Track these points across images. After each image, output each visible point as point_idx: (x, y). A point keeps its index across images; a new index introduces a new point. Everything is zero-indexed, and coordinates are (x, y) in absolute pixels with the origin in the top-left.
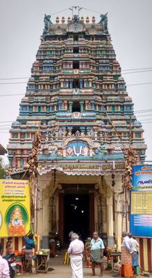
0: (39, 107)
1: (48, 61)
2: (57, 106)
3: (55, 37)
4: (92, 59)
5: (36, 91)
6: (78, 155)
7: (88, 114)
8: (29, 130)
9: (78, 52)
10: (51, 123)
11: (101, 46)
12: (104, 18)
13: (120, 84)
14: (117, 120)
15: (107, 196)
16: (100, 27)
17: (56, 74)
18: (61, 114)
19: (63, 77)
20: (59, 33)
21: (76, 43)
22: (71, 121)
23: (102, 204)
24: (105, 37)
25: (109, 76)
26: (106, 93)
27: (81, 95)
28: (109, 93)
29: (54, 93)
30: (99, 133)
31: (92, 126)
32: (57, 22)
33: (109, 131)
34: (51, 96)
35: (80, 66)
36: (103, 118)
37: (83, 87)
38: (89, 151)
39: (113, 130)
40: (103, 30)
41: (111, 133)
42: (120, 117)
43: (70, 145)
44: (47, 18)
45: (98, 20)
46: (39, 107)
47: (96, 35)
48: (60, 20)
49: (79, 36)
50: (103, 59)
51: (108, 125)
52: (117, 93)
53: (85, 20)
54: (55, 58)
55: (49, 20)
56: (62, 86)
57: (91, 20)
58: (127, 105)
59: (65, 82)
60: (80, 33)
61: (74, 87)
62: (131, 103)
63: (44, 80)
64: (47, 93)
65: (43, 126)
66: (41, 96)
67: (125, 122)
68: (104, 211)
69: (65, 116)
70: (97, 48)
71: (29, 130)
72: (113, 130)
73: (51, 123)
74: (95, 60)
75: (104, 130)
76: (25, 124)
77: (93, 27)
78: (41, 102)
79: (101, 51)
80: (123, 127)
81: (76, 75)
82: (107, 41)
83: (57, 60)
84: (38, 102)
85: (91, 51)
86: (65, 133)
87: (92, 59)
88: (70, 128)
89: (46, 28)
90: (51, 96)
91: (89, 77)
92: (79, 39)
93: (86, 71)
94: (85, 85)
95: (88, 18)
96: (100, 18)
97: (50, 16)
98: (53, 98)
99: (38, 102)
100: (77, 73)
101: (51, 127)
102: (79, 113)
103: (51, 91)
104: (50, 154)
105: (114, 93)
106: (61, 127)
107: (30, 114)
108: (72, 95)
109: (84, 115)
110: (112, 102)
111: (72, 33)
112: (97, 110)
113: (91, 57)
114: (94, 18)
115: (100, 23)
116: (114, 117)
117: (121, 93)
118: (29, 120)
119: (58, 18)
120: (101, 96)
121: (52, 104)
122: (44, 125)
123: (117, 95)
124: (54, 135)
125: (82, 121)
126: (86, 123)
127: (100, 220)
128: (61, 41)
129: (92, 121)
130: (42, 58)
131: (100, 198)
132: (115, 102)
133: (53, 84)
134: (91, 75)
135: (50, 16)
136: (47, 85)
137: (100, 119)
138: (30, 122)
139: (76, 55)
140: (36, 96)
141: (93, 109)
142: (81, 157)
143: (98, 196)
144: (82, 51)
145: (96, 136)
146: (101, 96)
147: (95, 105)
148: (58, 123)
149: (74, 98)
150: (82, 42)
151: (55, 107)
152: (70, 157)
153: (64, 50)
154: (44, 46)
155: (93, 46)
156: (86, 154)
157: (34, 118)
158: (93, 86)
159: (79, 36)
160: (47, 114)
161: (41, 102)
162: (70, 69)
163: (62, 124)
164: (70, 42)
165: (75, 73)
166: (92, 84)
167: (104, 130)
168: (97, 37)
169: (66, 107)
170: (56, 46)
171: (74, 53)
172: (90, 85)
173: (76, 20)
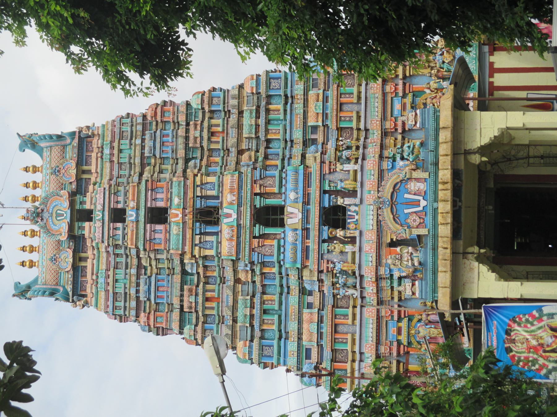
0: (265, 312)
1: (143, 288)
2: (263, 264)
3: (77, 270)
4: (141, 175)
5: (222, 320)
6: (423, 203)
7: (290, 185)
10: (310, 279)
11: (107, 151)
12: (30, 143)
13: (210, 103)
14: (305, 113)
15: (509, 144)
16: (56, 151)
17: (178, 269)
18: (289, 254)
19: (187, 248)
20: (67, 257)
21: (97, 215)
22: (306, 230)
23: (521, 154)
24: (83, 140)
25: (187, 131)
26: (232, 141)
27: (239, 205)
28: (233, 133)
29: (229, 274)
30: (338, 159)
31: (322, 177)
32: (32, 264)
34: (237, 281)
36: (297, 150)
37: (217, 198)
39: (332, 124)
40: (64, 147)
41: (340, 130)
42: (299, 107)
44: (23, 292)
45: (32, 158)
46: (265, 312)
49: (78, 207)
50: (143, 148)
51: (319, 137)
52: (235, 111)
53: (30, 192)
54: (134, 271)
60: (72, 204)
61: (216, 222)
62: (263, 79)
63: (192, 299)
64: (227, 293)
65: (317, 303)
66: (234, 308)
67: (312, 93)
68: (541, 151)
69: (295, 245)
70: (112, 162)
71: (326, 342)
72: (332, 124)
73: (310, 279)
75: (331, 146)
76: (308, 351)
77: (56, 172)
78: (252, 307)
79: (120, 151)
80: (326, 99)
82: (93, 135)
83: (139, 266)
86: (338, 247)
87: (141, 175)
89: (52, 294)
90: (237, 281)
91: (190, 182)
92: (87, 206)
93: (175, 190)
96: (29, 152)
98: (242, 276)
100: (179, 213)
101: (320, 281)
102: (289, 209)
103: (223, 280)
105: (233, 119)
107: (283, 336)
108: (239, 226)
109: (292, 196)
110: (257, 126)
112: (279, 163)
113: (136, 178)
114: (26, 169)
117: (233, 102)
118: (300, 339)
119: (23, 264)
120: (240, 152)
121: (257, 279)
122: (315, 299)
123: (241, 113)
125: (306, 202)
128: (89, 253)
129: (307, 177)
130: (133, 304)
131: (510, 160)
133: (197, 276)
136: (205, 291)
137: (303, 156)
138: (304, 337)
139: (131, 215)
140: (235, 321)
141: (277, 173)
145: (347, 167)
146: (240, 152)
147: (265, 168)
148: (312, 263)
149: (247, 220)
151: (266, 270)
153: (116, 246)
154: (102, 301)
155: (107, 171)
156: (421, 186)
157: (293, 326)
158: (214, 174)
159: (78, 207)
160: (284, 290)
161: (252, 307)
163: (313, 255)
164: (92, 230)
165: (133, 218)
166: (208, 175)
167: (331, 146)
168: (82, 160)
169: (268, 242)
170: (103, 267)
173: (36, 215)
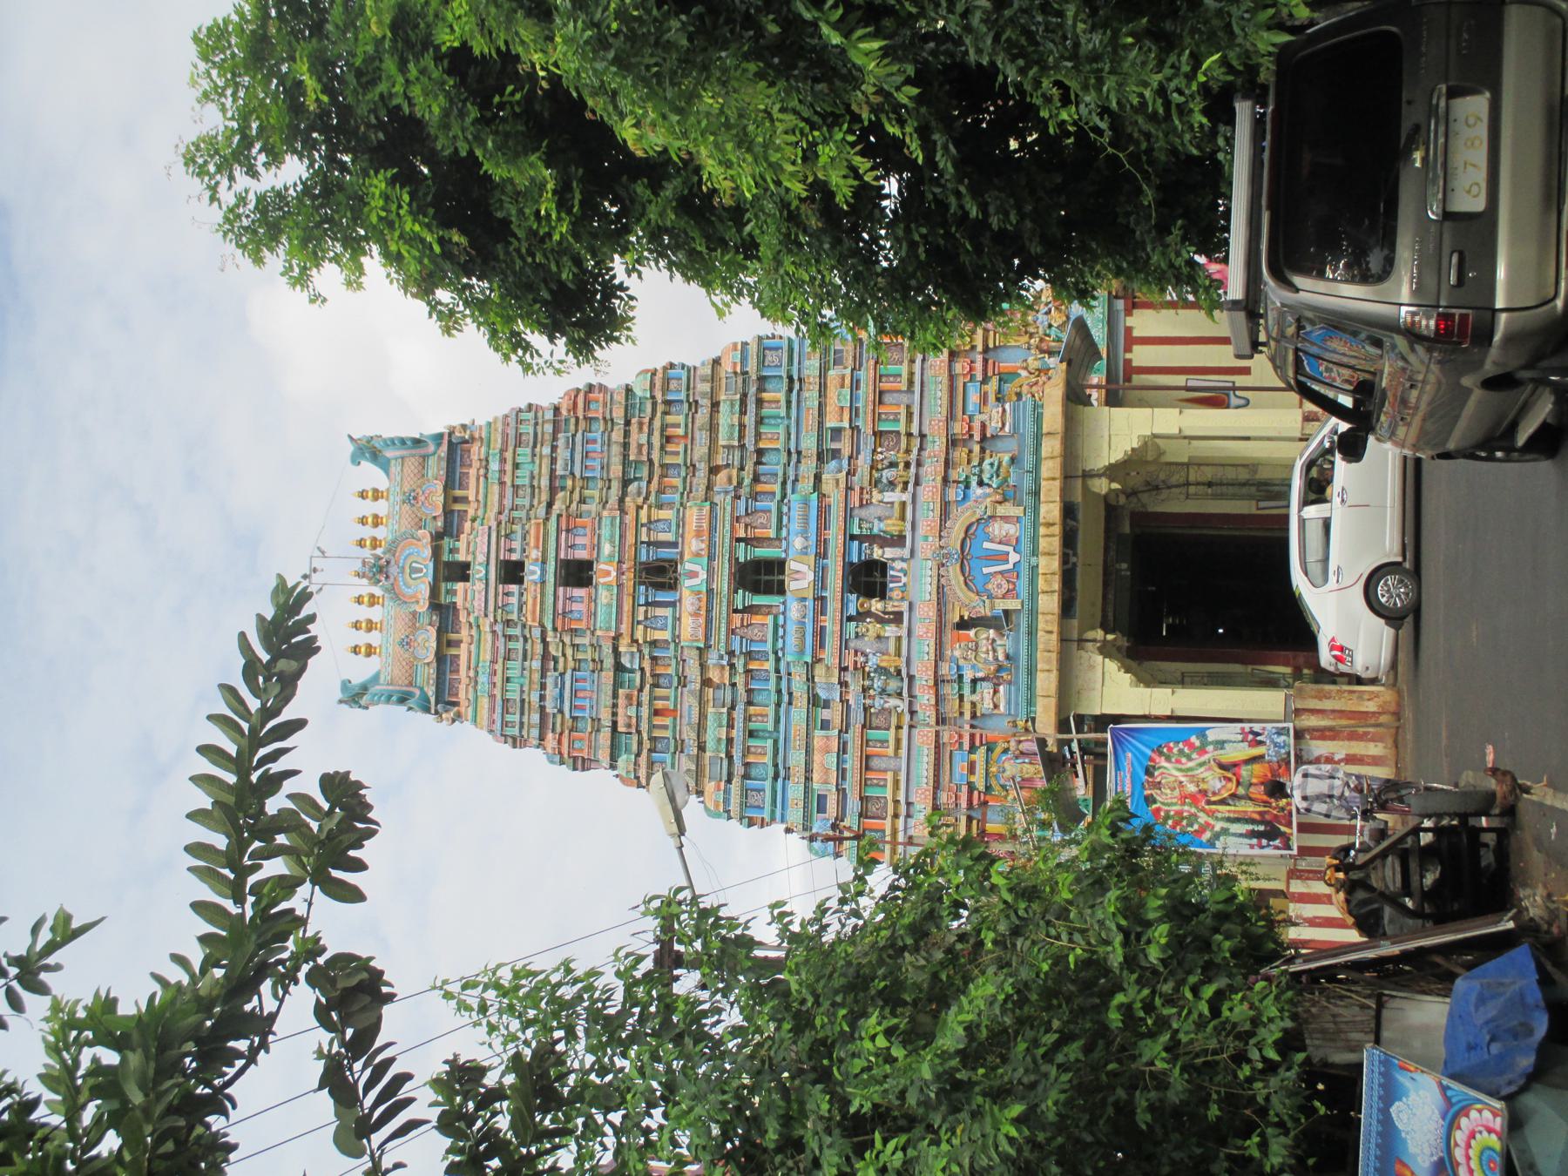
1: (551, 692)
3: (444, 661)
4: (550, 505)
5: (680, 747)
7: (795, 526)
8: (852, 785)
9: (519, 566)
12: (369, 450)
15: (1155, 461)
18: (792, 640)
20: (428, 639)
21: (477, 571)
24: (456, 447)
25: (627, 434)
26: (700, 450)
27: (711, 558)
28: (702, 438)
29: (693, 672)
30: (876, 483)
31: (848, 514)
33: (867, 443)
34: (706, 682)
35: (582, 554)
36: (808, 467)
37: (674, 545)
38: (1005, 519)
40: (425, 458)
42: (811, 396)
43: (979, 581)
45: (372, 476)
46: (752, 734)
47: (448, 486)
48: (362, 638)
50: (553, 461)
51: (845, 446)
52: (705, 402)
53: (368, 532)
54: (536, 664)
55: (364, 688)
56: (665, 635)
57: (369, 508)
58: (761, 362)
59: (649, 623)
61: (673, 586)
62: (753, 349)
63: (632, 712)
64: (690, 703)
66: (701, 728)
68: (1208, 474)
71: (852, 785)
74: (553, 491)
75: (863, 462)
76: (822, 799)
77: (411, 499)
78: (730, 726)
79: (516, 466)
81: (620, 573)
83: (546, 656)
84: (730, 741)
85: (514, 508)
87: (550, 505)
88: (854, 603)
90: (706, 682)
91: (630, 518)
93: (605, 532)
94: (663, 537)
95: (363, 521)
96: (367, 466)
97: (345, 685)
99: (730, 741)
103: (683, 682)
104: (1007, 657)
106: (844, 644)
109: (798, 543)
110: (742, 426)
111: (434, 591)
113: (541, 511)
114: (363, 495)
115: (385, 466)
116: (810, 420)
118: (808, 779)
119: (356, 650)
120: (714, 470)
122: (834, 714)
124: (881, 670)
126: (835, 535)
127: (1244, 490)
129: (823, 512)
130: (536, 718)
131: (1157, 488)
132: (743, 412)
133: (639, 672)
134: (623, 511)
135: (345, 685)
136: (652, 698)
137: (818, 478)
140: (702, 748)
141: (773, 506)
142: (1025, 546)
143: (1145, 498)
144: (517, 545)
145: (889, 496)
148: (830, 654)
150: (474, 546)
152: (1023, 585)
153: (508, 623)
156: (1012, 529)
157: (796, 759)
158: (670, 505)
159: (446, 557)
161: (730, 726)
162: (593, 600)
163: (832, 642)
164: (469, 596)
166: (660, 507)
167: (863, 462)
169: (757, 619)
171: (520, 581)
172: (665, 514)
173: (378, 571)
